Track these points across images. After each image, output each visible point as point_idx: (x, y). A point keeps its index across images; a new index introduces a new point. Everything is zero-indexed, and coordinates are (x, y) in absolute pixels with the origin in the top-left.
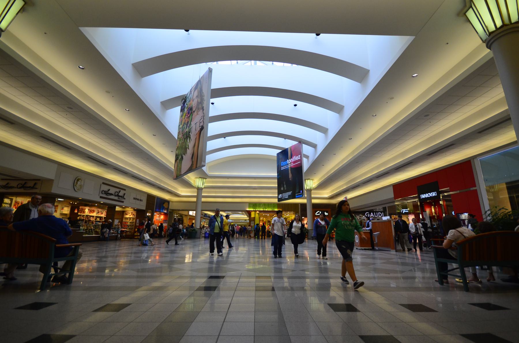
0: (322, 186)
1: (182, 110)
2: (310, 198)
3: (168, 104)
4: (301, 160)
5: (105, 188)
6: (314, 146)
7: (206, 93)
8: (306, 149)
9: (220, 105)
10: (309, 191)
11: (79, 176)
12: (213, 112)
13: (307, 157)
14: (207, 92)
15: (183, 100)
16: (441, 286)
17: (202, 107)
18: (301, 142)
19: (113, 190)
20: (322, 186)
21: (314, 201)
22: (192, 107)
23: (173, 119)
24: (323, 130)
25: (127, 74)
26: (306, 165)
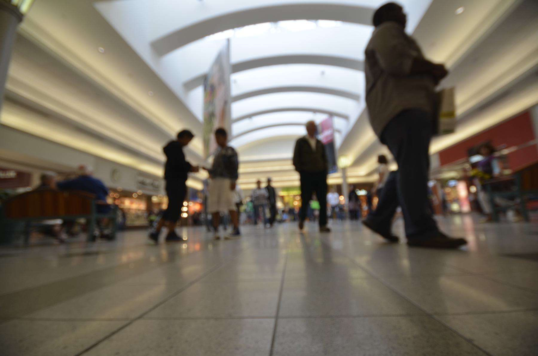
0: (359, 161)
1: (205, 90)
2: (345, 177)
3: (190, 85)
4: (332, 135)
5: (141, 179)
6: (345, 117)
7: (227, 69)
8: (338, 123)
9: (241, 82)
10: (344, 170)
11: (116, 168)
12: (235, 91)
13: (339, 131)
14: (227, 66)
15: (204, 80)
16: (525, 225)
17: (224, 82)
18: (331, 114)
19: (148, 181)
20: (359, 161)
21: (351, 180)
22: (213, 83)
23: (196, 100)
24: (345, 117)
25: (144, 52)
26: (338, 140)
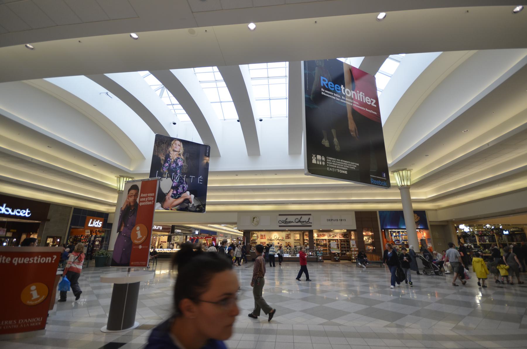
5: (283, 218)
19: (290, 218)
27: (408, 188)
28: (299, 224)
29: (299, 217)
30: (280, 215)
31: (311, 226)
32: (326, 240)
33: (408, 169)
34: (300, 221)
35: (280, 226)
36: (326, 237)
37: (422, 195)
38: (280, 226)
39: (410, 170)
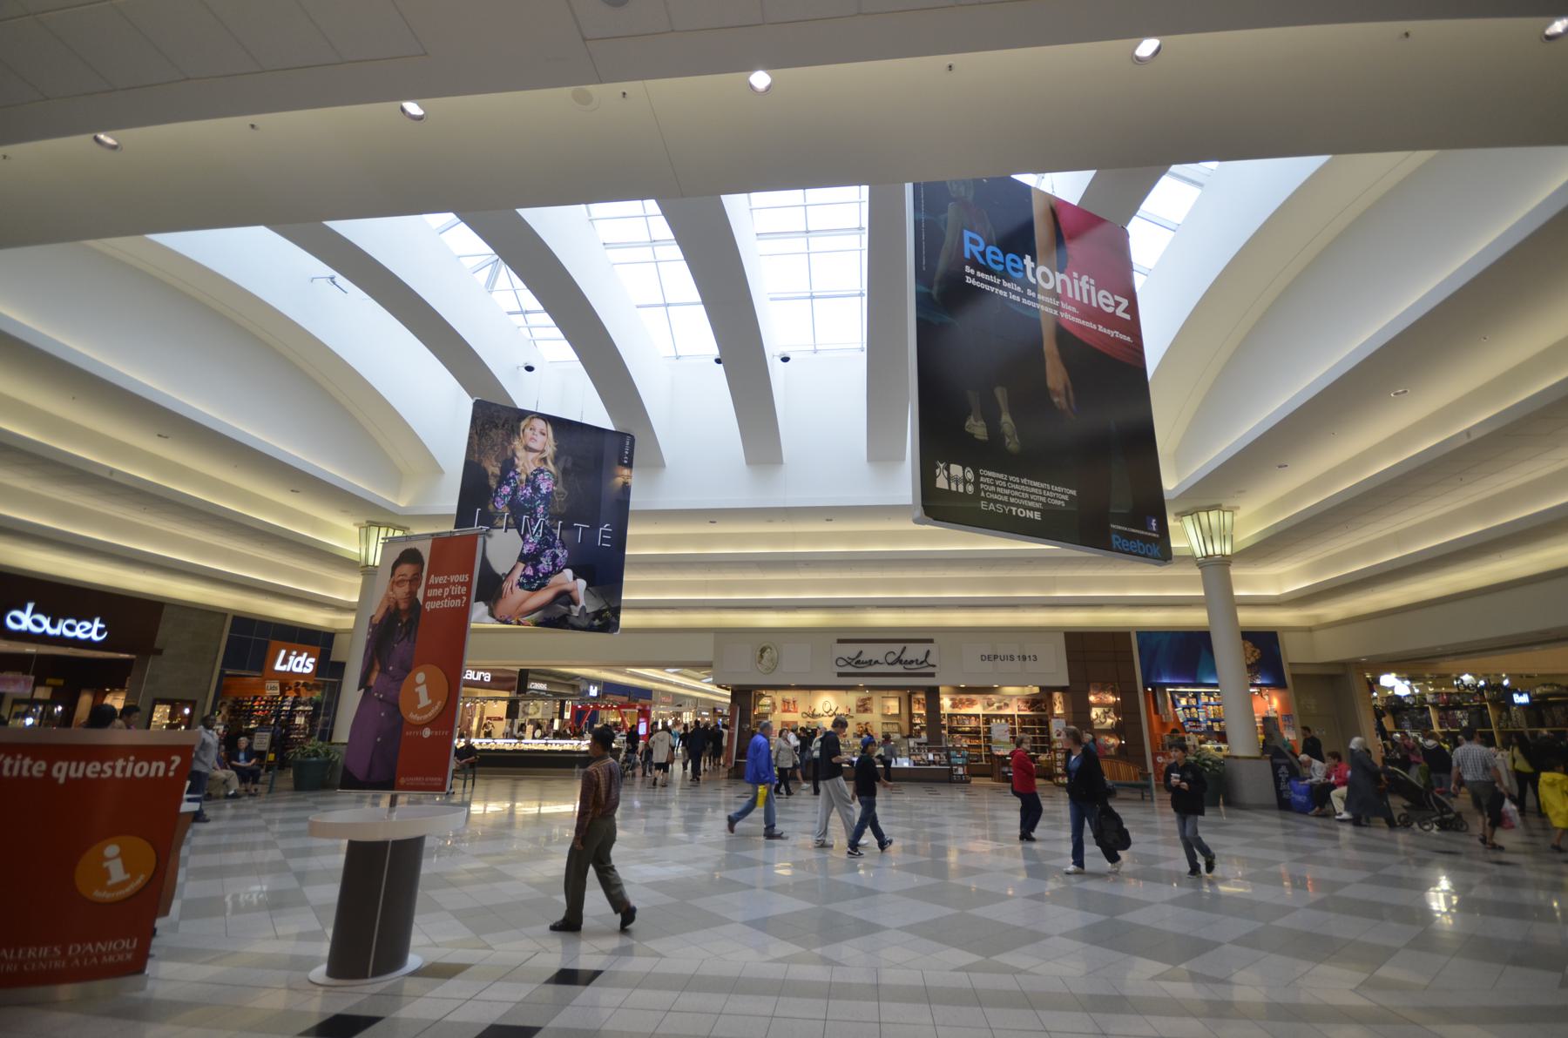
5: (851, 651)
19: (871, 652)
27: (1224, 562)
28: (898, 668)
29: (897, 648)
30: (840, 641)
31: (932, 675)
32: (977, 716)
33: (1225, 505)
34: (899, 661)
35: (840, 675)
36: (978, 709)
37: (1269, 586)
38: (840, 675)
39: (1232, 510)
